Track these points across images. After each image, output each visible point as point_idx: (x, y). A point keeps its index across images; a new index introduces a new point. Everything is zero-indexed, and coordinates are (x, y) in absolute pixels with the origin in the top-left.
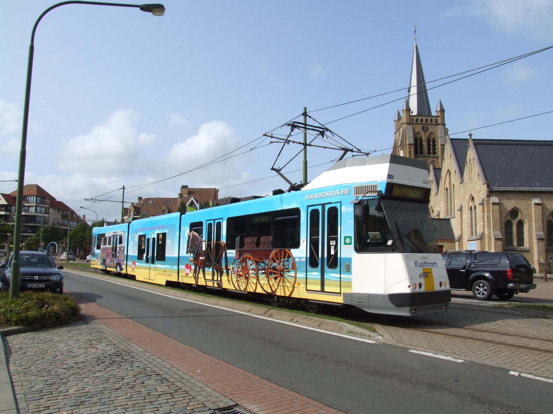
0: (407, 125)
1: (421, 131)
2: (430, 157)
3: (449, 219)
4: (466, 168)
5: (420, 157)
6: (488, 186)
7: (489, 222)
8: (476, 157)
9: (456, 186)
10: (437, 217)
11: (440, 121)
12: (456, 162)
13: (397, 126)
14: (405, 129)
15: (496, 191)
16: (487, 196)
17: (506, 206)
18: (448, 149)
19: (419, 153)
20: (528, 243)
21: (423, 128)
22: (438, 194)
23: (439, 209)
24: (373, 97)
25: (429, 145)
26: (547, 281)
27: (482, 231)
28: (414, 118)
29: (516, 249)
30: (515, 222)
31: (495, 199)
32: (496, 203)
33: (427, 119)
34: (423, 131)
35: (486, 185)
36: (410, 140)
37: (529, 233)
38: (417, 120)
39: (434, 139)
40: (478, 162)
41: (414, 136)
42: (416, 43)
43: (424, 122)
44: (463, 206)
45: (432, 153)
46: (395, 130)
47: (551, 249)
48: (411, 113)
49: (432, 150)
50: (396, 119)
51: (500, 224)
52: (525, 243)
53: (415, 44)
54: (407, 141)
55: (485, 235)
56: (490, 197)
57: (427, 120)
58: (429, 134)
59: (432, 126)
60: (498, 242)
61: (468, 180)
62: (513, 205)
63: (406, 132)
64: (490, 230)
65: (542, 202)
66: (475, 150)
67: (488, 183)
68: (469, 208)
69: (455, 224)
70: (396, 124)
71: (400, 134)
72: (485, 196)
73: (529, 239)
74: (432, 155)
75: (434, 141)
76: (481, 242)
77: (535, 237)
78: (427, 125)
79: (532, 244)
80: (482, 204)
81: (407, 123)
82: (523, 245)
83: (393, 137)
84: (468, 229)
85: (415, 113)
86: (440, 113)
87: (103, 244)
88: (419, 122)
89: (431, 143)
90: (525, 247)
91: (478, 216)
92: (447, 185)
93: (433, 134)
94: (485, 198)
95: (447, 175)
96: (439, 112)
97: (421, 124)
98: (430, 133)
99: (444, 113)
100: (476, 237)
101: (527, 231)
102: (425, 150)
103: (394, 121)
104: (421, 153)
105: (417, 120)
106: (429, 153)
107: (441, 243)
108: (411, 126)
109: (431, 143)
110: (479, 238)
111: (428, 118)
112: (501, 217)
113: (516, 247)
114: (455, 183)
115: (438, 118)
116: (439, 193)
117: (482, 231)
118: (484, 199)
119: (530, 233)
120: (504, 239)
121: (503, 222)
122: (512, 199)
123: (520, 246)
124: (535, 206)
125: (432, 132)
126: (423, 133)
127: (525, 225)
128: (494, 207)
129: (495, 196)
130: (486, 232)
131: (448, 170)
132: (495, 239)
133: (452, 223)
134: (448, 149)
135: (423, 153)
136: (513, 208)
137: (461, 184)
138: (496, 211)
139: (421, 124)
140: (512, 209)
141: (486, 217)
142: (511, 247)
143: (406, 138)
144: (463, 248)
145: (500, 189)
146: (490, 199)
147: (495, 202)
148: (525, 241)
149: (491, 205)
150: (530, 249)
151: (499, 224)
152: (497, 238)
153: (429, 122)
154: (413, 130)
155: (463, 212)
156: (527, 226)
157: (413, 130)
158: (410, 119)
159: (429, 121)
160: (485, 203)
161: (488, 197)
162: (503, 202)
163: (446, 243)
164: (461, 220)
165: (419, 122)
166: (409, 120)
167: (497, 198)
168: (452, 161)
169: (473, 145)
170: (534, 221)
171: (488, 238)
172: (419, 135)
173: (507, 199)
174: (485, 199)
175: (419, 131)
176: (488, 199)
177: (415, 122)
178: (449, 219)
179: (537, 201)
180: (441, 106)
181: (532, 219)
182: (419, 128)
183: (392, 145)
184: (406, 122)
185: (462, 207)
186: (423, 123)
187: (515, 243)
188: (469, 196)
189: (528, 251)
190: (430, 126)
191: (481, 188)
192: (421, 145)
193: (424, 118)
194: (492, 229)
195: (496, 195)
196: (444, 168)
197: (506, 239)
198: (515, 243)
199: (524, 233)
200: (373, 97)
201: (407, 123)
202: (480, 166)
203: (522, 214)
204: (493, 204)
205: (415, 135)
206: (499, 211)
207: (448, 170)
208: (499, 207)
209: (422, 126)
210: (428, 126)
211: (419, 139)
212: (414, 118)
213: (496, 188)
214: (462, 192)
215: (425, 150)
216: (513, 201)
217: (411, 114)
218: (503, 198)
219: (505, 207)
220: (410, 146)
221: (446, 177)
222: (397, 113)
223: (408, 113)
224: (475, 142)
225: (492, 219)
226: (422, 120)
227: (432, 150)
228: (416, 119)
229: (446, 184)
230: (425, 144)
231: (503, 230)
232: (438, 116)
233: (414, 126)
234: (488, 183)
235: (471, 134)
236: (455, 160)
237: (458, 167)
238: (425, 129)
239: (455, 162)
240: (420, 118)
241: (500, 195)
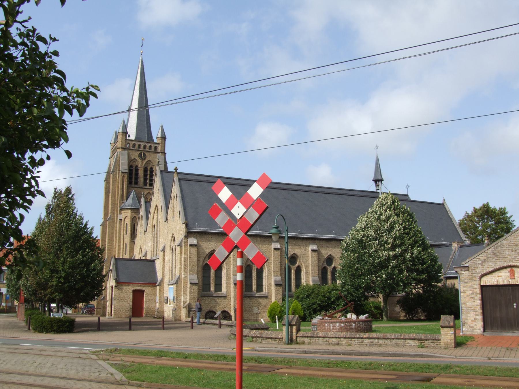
0: (122, 150)
1: (137, 158)
2: (145, 188)
3: (153, 261)
4: (170, 205)
5: (134, 187)
6: (187, 225)
7: (185, 265)
8: (179, 194)
9: (161, 224)
10: (144, 258)
11: (160, 149)
12: (164, 197)
13: (113, 149)
14: (120, 155)
15: (195, 232)
16: (186, 237)
17: (205, 249)
18: (158, 182)
19: (133, 182)
20: (225, 288)
21: (140, 155)
22: (146, 231)
23: (146, 248)
24: (201, 99)
25: (145, 175)
26: (220, 328)
27: (179, 275)
28: (130, 142)
29: (213, 294)
30: (293, 268)
31: (193, 241)
32: (194, 245)
33: (145, 145)
34: (139, 158)
35: (184, 225)
36: (124, 167)
37: (226, 278)
38: (134, 145)
39: (151, 168)
40: (180, 199)
41: (129, 163)
42: (142, 58)
43: (142, 149)
44: (166, 246)
45: (148, 184)
46: (111, 154)
47: (248, 294)
48: (127, 137)
49: (148, 181)
50: (113, 142)
51: (197, 268)
52: (223, 288)
53: (141, 59)
54: (120, 168)
55: (181, 279)
56: (188, 239)
57: (145, 147)
58: (146, 163)
59: (151, 154)
60: (194, 286)
61: (172, 218)
62: (212, 247)
63: (119, 158)
64: (186, 274)
65: (281, 247)
66: (179, 186)
67: (187, 223)
68: (171, 249)
69: (158, 264)
70: (112, 147)
71: (114, 157)
72: (183, 237)
73: (226, 284)
74: (148, 187)
75: (152, 171)
76: (177, 286)
77: (232, 281)
78: (144, 152)
79: (229, 290)
80: (180, 245)
81: (122, 148)
82: (221, 290)
83: (108, 162)
84: (169, 272)
85: (133, 137)
86: (160, 141)
87: (236, 358)
88: (136, 148)
89: (148, 173)
90: (222, 292)
91: (177, 258)
92: (155, 223)
93: (152, 163)
94: (184, 239)
95: (155, 210)
96: (160, 139)
97: (139, 150)
98: (147, 162)
99: (165, 140)
100: (173, 281)
101: (225, 275)
102: (141, 180)
103: (111, 143)
104: (136, 183)
105: (134, 145)
106: (145, 184)
107: (141, 287)
108: (126, 152)
109: (148, 173)
110: (174, 282)
111: (147, 144)
112: (198, 260)
113: (214, 292)
114: (161, 220)
115: (157, 146)
116: (147, 231)
117: (179, 275)
118: (182, 239)
119: (228, 277)
120: (201, 284)
121: (201, 265)
122: (211, 241)
123: (218, 291)
124: (275, 251)
125: (149, 161)
126: (139, 161)
127: (223, 269)
128: (192, 249)
129: (194, 237)
130: (183, 276)
131: (156, 206)
132: (191, 283)
133: (156, 264)
134: (158, 182)
135: (138, 184)
136: (212, 251)
137: (165, 221)
138: (193, 253)
139: (139, 150)
140: (211, 252)
141: (183, 259)
142: (208, 293)
143: (119, 164)
144: (164, 293)
145: (199, 229)
146: (188, 240)
147: (192, 244)
148: (223, 286)
149: (189, 247)
150: (227, 295)
151: (196, 267)
152: (193, 282)
153: (147, 149)
154: (129, 156)
155: (166, 253)
156: (225, 270)
157: (128, 156)
158: (127, 143)
159: (148, 147)
160: (183, 244)
161: (186, 237)
162: (202, 244)
163: (147, 288)
164: (163, 262)
165: (136, 148)
166: (125, 144)
167: (196, 239)
168: (160, 196)
169: (177, 180)
170: (232, 265)
171: (184, 282)
172: (135, 162)
173: (206, 241)
174: (183, 240)
175: (135, 157)
176: (186, 240)
177: (131, 148)
178: (153, 261)
179: (315, 247)
180: (163, 132)
181: (231, 263)
182: (135, 155)
183: (106, 171)
184: (122, 146)
185: (164, 247)
186: (141, 149)
187: (212, 289)
188: (171, 236)
189: (225, 297)
190: (149, 154)
191: (180, 227)
192: (137, 174)
193: (142, 144)
194: (188, 273)
195: (195, 236)
196: (153, 203)
197: (203, 284)
198: (212, 289)
199: (222, 277)
200: (201, 99)
201: (122, 148)
202: (182, 204)
203: (300, 261)
204: (191, 245)
205: (131, 161)
206: (196, 253)
207: (156, 206)
208: (196, 249)
209: (140, 152)
210: (146, 154)
211: (134, 168)
212: (130, 142)
213: (195, 229)
214: (166, 231)
215: (141, 180)
216: (212, 243)
217: (128, 138)
218: (202, 239)
219: (204, 250)
220: (123, 175)
221: (154, 212)
222: (161, 129)
223: (125, 136)
224: (181, 176)
225: (189, 262)
226: (139, 146)
227: (148, 181)
228: (132, 144)
229: (154, 220)
230: (141, 173)
231: (200, 274)
232: (159, 144)
233: (130, 151)
234: (187, 223)
235: (177, 168)
236: (162, 195)
237: (165, 202)
238: (142, 156)
239: (162, 198)
240: (137, 144)
241: (199, 237)
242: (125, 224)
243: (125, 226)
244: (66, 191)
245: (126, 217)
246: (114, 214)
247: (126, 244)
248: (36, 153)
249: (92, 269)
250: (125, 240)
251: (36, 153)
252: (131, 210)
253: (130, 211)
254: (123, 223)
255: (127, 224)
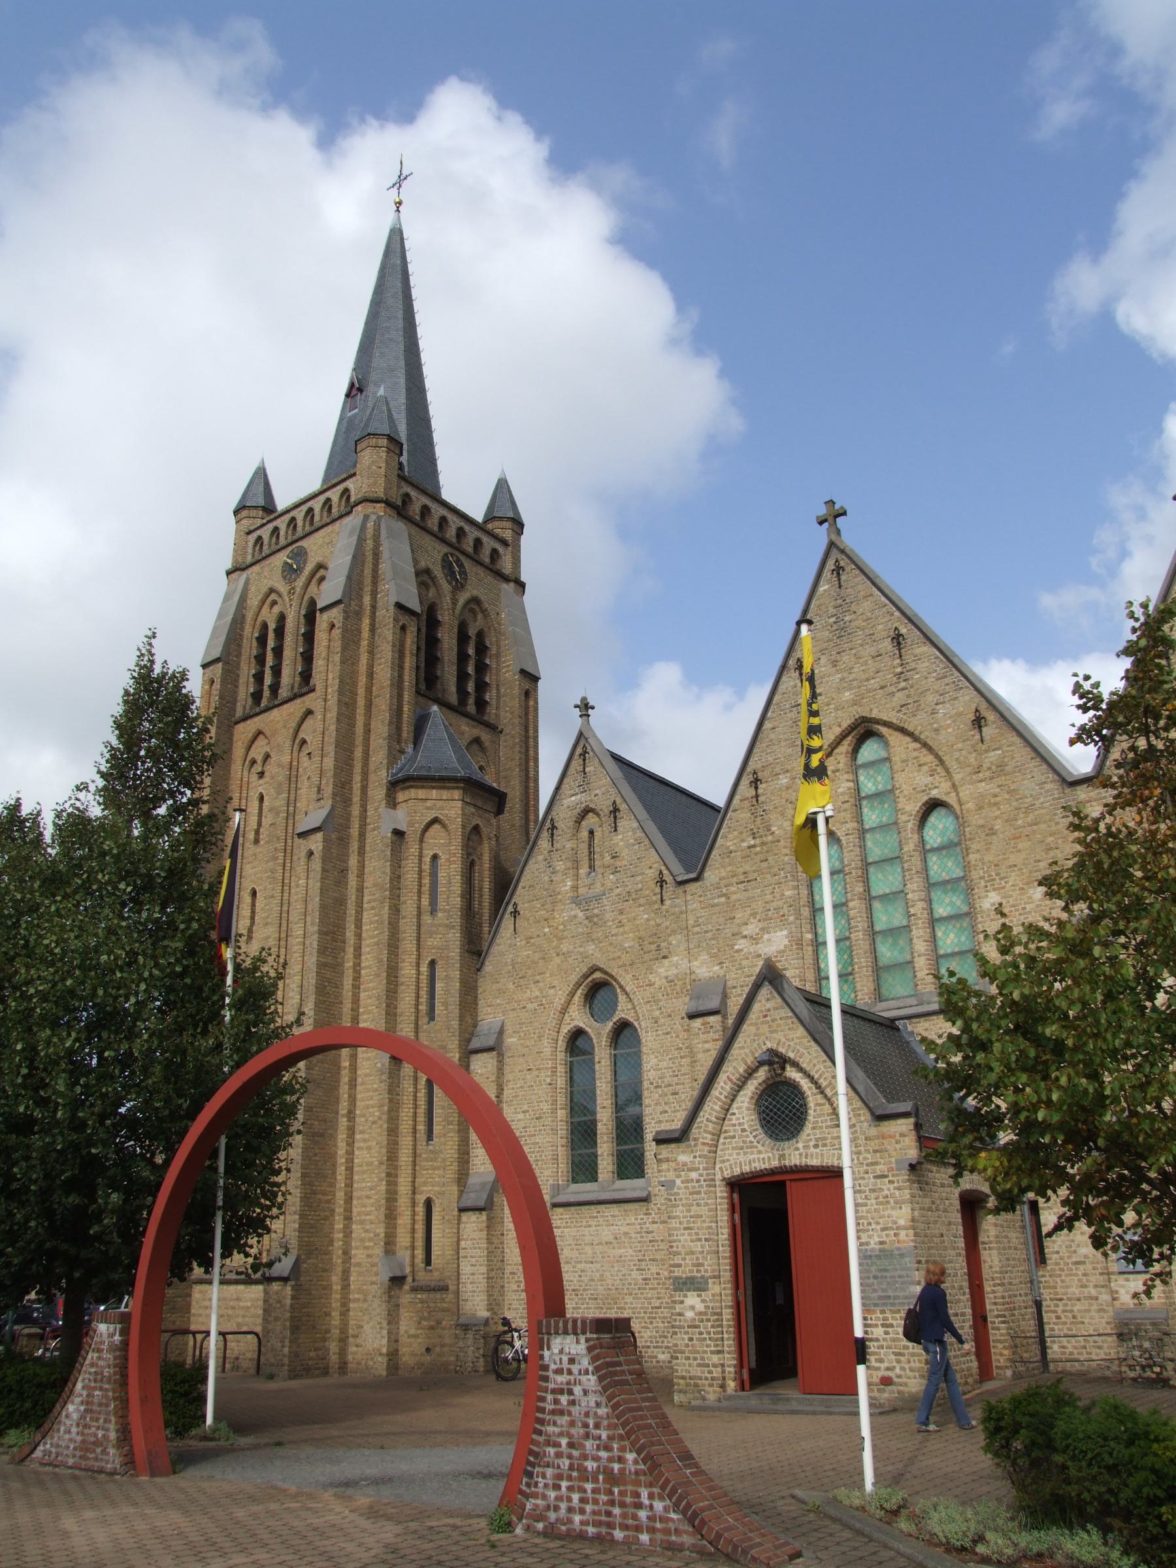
39: (480, 635)
76: (489, 1219)
81: (388, 503)
175: (431, 566)
242: (427, 859)
243: (426, 867)
244: (120, 737)
245: (435, 821)
246: (347, 802)
247: (433, 963)
248: (17, 806)
249: (1078, 1219)
250: (432, 943)
251: (17, 806)
252: (465, 790)
253: (457, 794)
254: (413, 849)
255: (435, 857)
